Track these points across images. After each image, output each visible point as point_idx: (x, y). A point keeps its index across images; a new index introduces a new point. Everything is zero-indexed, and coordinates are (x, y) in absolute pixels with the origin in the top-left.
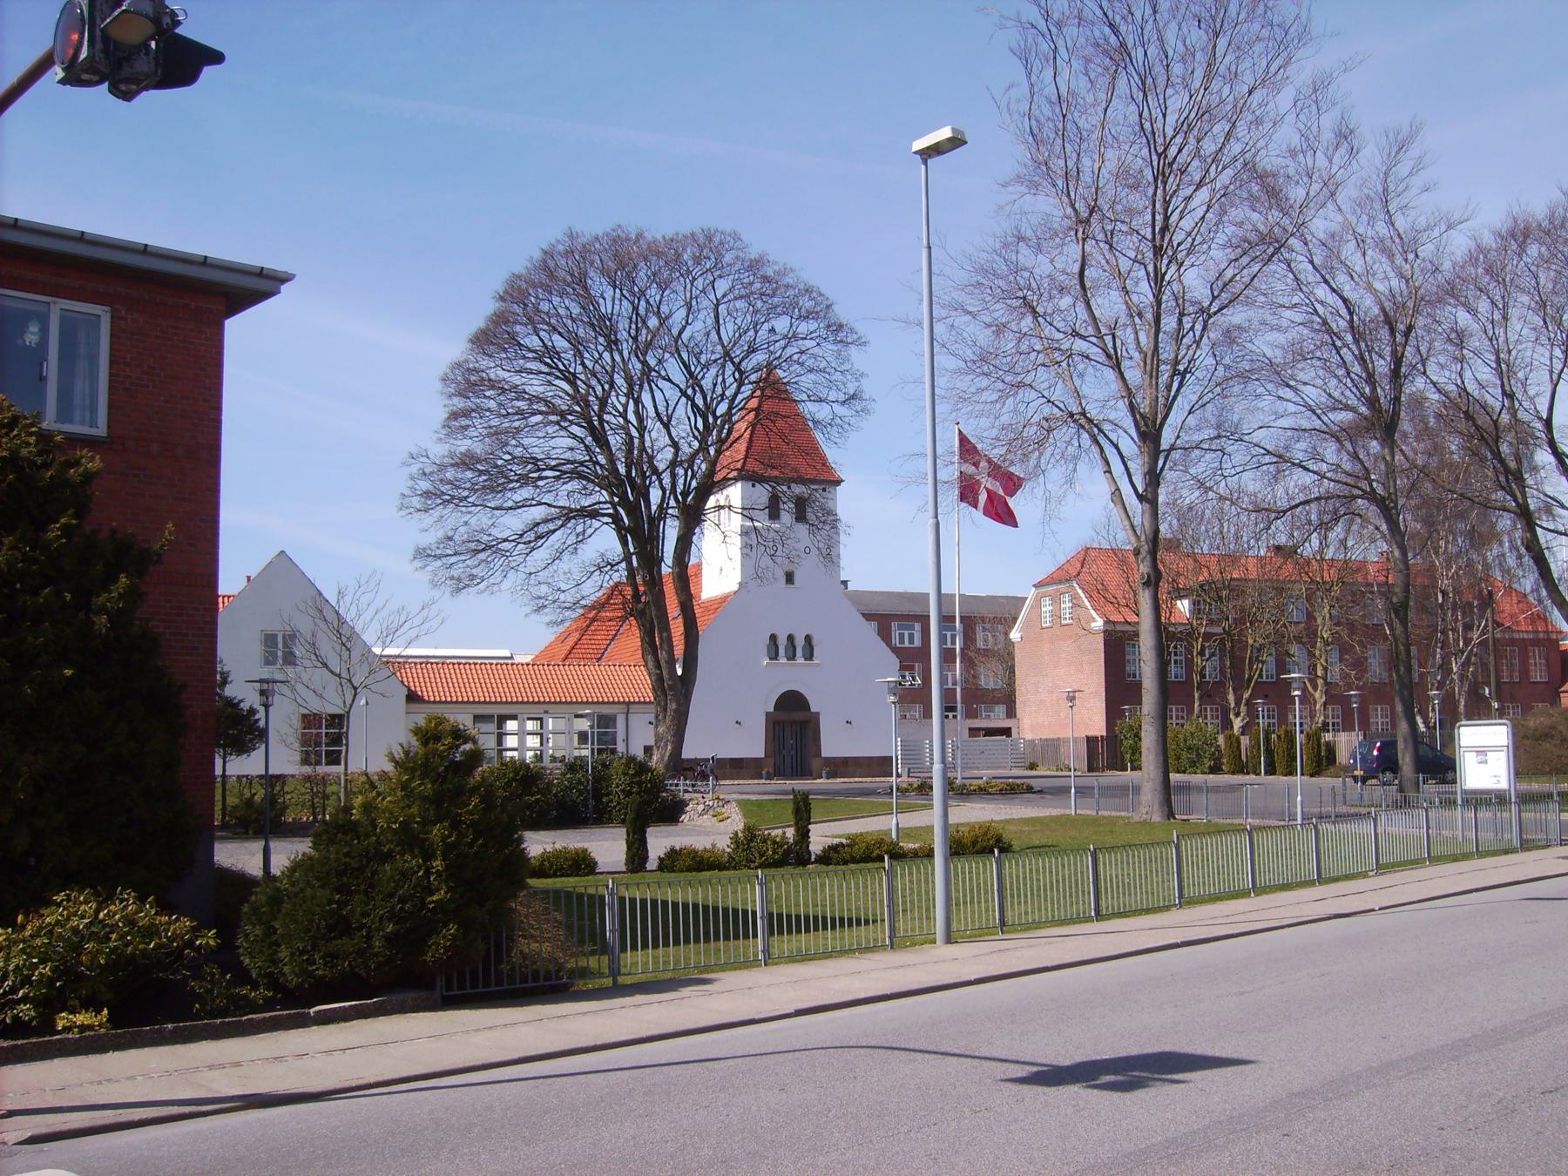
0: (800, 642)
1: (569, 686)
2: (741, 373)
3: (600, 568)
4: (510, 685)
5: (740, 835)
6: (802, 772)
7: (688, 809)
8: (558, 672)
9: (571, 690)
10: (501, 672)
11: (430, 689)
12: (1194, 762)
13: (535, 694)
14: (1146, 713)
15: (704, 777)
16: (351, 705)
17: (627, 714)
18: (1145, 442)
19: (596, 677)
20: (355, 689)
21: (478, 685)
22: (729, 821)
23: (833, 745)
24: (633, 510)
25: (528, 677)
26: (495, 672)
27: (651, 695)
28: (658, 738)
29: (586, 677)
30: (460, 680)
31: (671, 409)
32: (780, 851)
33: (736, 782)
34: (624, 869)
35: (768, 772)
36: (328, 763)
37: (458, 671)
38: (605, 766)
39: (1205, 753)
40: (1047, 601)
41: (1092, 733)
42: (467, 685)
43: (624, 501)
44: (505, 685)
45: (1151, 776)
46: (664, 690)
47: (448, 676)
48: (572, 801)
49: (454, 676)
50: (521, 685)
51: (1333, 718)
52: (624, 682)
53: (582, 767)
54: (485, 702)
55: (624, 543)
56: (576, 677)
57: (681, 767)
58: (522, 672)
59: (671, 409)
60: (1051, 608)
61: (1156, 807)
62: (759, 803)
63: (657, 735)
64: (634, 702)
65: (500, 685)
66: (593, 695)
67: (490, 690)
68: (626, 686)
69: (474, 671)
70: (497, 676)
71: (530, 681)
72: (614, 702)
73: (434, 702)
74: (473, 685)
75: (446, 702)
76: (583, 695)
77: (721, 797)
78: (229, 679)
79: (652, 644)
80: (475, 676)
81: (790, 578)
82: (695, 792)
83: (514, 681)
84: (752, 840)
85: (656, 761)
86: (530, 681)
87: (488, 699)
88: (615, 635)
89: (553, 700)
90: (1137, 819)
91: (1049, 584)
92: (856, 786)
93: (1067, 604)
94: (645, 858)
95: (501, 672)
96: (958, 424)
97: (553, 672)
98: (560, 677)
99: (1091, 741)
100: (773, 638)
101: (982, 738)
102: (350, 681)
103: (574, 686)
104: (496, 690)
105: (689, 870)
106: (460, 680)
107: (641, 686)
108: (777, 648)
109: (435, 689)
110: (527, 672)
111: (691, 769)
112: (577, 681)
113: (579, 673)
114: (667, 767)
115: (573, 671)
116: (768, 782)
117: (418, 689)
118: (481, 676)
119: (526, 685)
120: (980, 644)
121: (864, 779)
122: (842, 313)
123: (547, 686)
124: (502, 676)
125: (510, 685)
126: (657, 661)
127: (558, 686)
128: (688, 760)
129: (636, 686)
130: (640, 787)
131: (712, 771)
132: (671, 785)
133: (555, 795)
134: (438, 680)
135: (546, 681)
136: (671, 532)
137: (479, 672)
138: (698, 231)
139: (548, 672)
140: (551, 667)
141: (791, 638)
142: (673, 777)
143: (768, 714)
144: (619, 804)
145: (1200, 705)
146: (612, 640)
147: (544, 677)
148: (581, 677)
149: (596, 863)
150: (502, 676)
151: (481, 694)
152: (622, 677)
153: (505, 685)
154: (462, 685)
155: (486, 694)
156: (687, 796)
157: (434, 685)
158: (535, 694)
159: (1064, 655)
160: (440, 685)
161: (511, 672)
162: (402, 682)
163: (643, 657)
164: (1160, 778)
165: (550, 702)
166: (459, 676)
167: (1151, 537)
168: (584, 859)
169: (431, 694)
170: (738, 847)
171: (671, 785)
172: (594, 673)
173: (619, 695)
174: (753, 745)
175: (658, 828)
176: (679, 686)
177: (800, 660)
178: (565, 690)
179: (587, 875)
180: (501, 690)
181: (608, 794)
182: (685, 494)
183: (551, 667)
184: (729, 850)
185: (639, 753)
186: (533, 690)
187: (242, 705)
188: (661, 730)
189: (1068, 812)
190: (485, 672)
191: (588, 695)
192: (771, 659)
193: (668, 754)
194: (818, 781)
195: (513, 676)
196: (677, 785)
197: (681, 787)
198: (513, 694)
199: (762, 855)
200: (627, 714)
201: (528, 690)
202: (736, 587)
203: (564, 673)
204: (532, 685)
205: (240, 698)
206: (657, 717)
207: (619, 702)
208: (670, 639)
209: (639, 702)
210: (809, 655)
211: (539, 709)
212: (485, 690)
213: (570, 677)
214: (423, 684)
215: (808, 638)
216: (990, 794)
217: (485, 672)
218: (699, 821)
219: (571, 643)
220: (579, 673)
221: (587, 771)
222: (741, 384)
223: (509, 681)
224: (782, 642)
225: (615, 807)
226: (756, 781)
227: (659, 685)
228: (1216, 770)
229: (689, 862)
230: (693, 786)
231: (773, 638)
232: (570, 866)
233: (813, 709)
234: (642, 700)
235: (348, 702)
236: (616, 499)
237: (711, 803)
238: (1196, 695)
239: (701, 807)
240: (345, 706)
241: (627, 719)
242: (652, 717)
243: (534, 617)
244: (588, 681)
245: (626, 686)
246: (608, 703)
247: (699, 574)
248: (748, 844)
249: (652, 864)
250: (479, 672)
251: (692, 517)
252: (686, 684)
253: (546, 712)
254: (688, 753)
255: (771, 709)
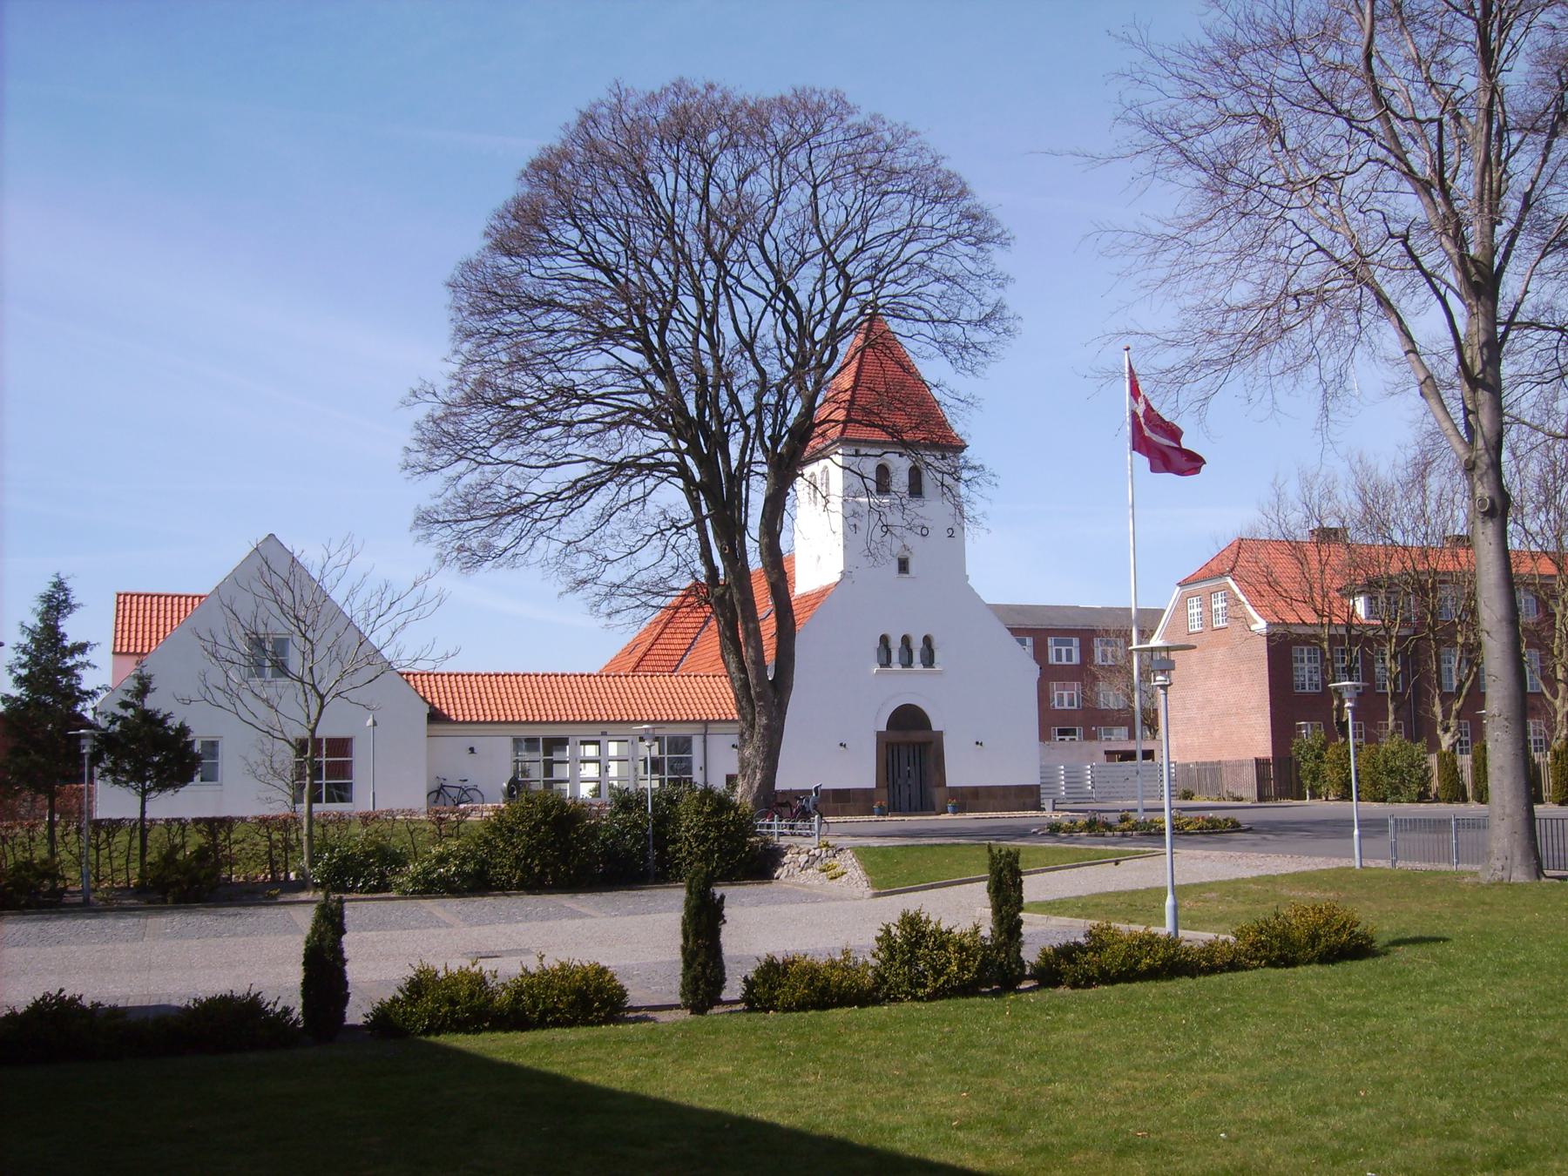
0: (917, 646)
1: (632, 701)
2: (848, 278)
3: (662, 532)
4: (560, 701)
5: (894, 930)
6: (924, 805)
7: (785, 860)
8: (619, 685)
9: (634, 707)
10: (548, 685)
11: (458, 706)
12: (1397, 788)
13: (590, 712)
14: (1496, 712)
15: (805, 815)
16: (317, 720)
17: (705, 735)
18: (1478, 299)
19: (666, 690)
20: (322, 697)
21: (519, 701)
22: (844, 878)
23: (960, 771)
24: (706, 463)
25: (582, 690)
26: (541, 685)
27: (734, 711)
28: (744, 764)
29: (654, 690)
30: (497, 695)
31: (755, 323)
32: (974, 965)
33: (842, 819)
34: (678, 1000)
35: (880, 807)
36: (330, 799)
37: (495, 684)
38: (672, 802)
39: (1411, 777)
40: (1195, 601)
41: (1261, 756)
42: (506, 701)
43: (694, 450)
44: (553, 701)
45: (1508, 811)
46: (750, 700)
47: (482, 690)
48: (624, 850)
49: (489, 690)
50: (573, 701)
51: (1535, 734)
52: (700, 695)
53: (639, 803)
54: (527, 722)
55: (696, 507)
56: (641, 690)
57: (775, 802)
58: (574, 685)
59: (755, 323)
60: (1200, 610)
61: (1518, 858)
62: (884, 852)
63: (742, 760)
64: (714, 721)
65: (546, 701)
66: (663, 712)
67: (535, 707)
68: (703, 701)
69: (515, 684)
70: (543, 690)
71: (584, 695)
72: (688, 721)
73: (464, 722)
74: (512, 701)
75: (478, 722)
76: (650, 712)
77: (831, 843)
78: (152, 686)
79: (734, 640)
80: (516, 690)
81: (903, 566)
82: (793, 835)
83: (564, 696)
84: (917, 944)
85: (742, 795)
86: (584, 695)
87: (531, 719)
88: (692, 644)
89: (612, 718)
90: (1485, 878)
91: (1205, 579)
92: (1010, 822)
93: (1219, 605)
94: (718, 982)
95: (548, 685)
96: (1128, 349)
97: (613, 685)
98: (622, 690)
99: (1260, 764)
100: (884, 640)
101: (1117, 763)
102: (314, 686)
103: (639, 701)
104: (541, 707)
105: (802, 1006)
106: (497, 695)
107: (722, 701)
108: (889, 652)
109: (465, 706)
110: (581, 685)
111: (787, 804)
112: (643, 695)
113: (645, 685)
114: (755, 800)
115: (638, 682)
116: (881, 818)
117: (444, 706)
118: (523, 690)
119: (579, 701)
120: (1098, 659)
121: (999, 814)
122: (984, 195)
123: (606, 701)
124: (550, 690)
125: (560, 701)
126: (741, 662)
127: (619, 701)
128: (784, 793)
129: (716, 701)
130: (720, 831)
131: (815, 807)
132: (762, 826)
133: (603, 842)
134: (470, 695)
135: (604, 696)
136: (757, 494)
137: (521, 684)
138: (788, 94)
139: (606, 685)
140: (610, 679)
141: (906, 640)
142: (763, 815)
143: (879, 734)
144: (690, 853)
145: (1395, 719)
146: (689, 649)
147: (602, 690)
148: (647, 690)
149: (623, 994)
150: (550, 690)
151: (522, 712)
152: (698, 690)
153: (553, 701)
154: (499, 701)
155: (529, 712)
156: (784, 841)
157: (464, 701)
158: (590, 712)
159: (1217, 665)
160: (471, 701)
161: (561, 685)
162: (424, 698)
163: (723, 657)
164: (1520, 817)
165: (608, 722)
166: (496, 690)
167: (1493, 441)
168: (599, 990)
169: (460, 712)
170: (892, 958)
171: (762, 826)
172: (664, 685)
173: (695, 711)
174: (861, 773)
175: (741, 888)
176: (770, 693)
177: (918, 666)
178: (628, 706)
179: (606, 1021)
180: (548, 707)
181: (674, 841)
182: (775, 439)
183: (610, 679)
184: (873, 962)
185: (719, 784)
186: (588, 706)
187: (170, 722)
188: (747, 752)
189: (1344, 863)
190: (528, 684)
191: (656, 712)
192: (882, 666)
193: (756, 785)
194: (942, 817)
195: (563, 690)
196: (769, 826)
197: (775, 830)
198: (563, 712)
199: (938, 973)
200: (705, 735)
201: (581, 706)
202: (837, 578)
203: (626, 685)
204: (586, 701)
205: (165, 711)
206: (742, 735)
207: (694, 721)
208: (757, 631)
209: (720, 721)
210: (929, 660)
211: (600, 729)
212: (528, 707)
213: (635, 690)
214: (450, 701)
215: (927, 640)
216: (1188, 833)
217: (528, 684)
218: (802, 878)
219: (640, 654)
220: (645, 685)
221: (647, 808)
222: (846, 295)
223: (558, 696)
224: (895, 645)
225: (684, 859)
226: (866, 818)
227: (744, 694)
228: (1422, 797)
229: (801, 991)
230: (792, 827)
231: (884, 640)
232: (572, 1005)
233: (934, 728)
234: (723, 717)
235: (313, 716)
236: (684, 445)
237: (817, 852)
238: (1391, 707)
239: (803, 858)
240: (309, 722)
241: (705, 741)
242: (735, 740)
243: (569, 596)
244: (656, 695)
245: (703, 701)
246: (681, 721)
247: (792, 559)
248: (912, 953)
249: (733, 989)
250: (521, 684)
251: (785, 471)
252: (780, 687)
253: (604, 734)
254: (782, 784)
255: (884, 728)
